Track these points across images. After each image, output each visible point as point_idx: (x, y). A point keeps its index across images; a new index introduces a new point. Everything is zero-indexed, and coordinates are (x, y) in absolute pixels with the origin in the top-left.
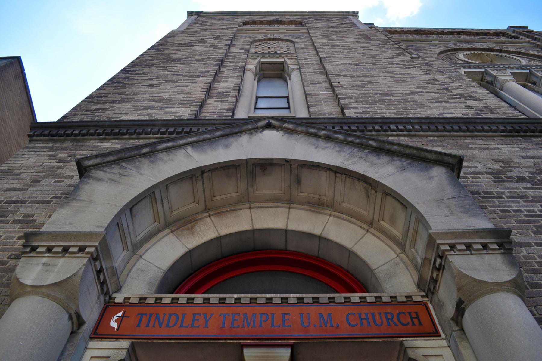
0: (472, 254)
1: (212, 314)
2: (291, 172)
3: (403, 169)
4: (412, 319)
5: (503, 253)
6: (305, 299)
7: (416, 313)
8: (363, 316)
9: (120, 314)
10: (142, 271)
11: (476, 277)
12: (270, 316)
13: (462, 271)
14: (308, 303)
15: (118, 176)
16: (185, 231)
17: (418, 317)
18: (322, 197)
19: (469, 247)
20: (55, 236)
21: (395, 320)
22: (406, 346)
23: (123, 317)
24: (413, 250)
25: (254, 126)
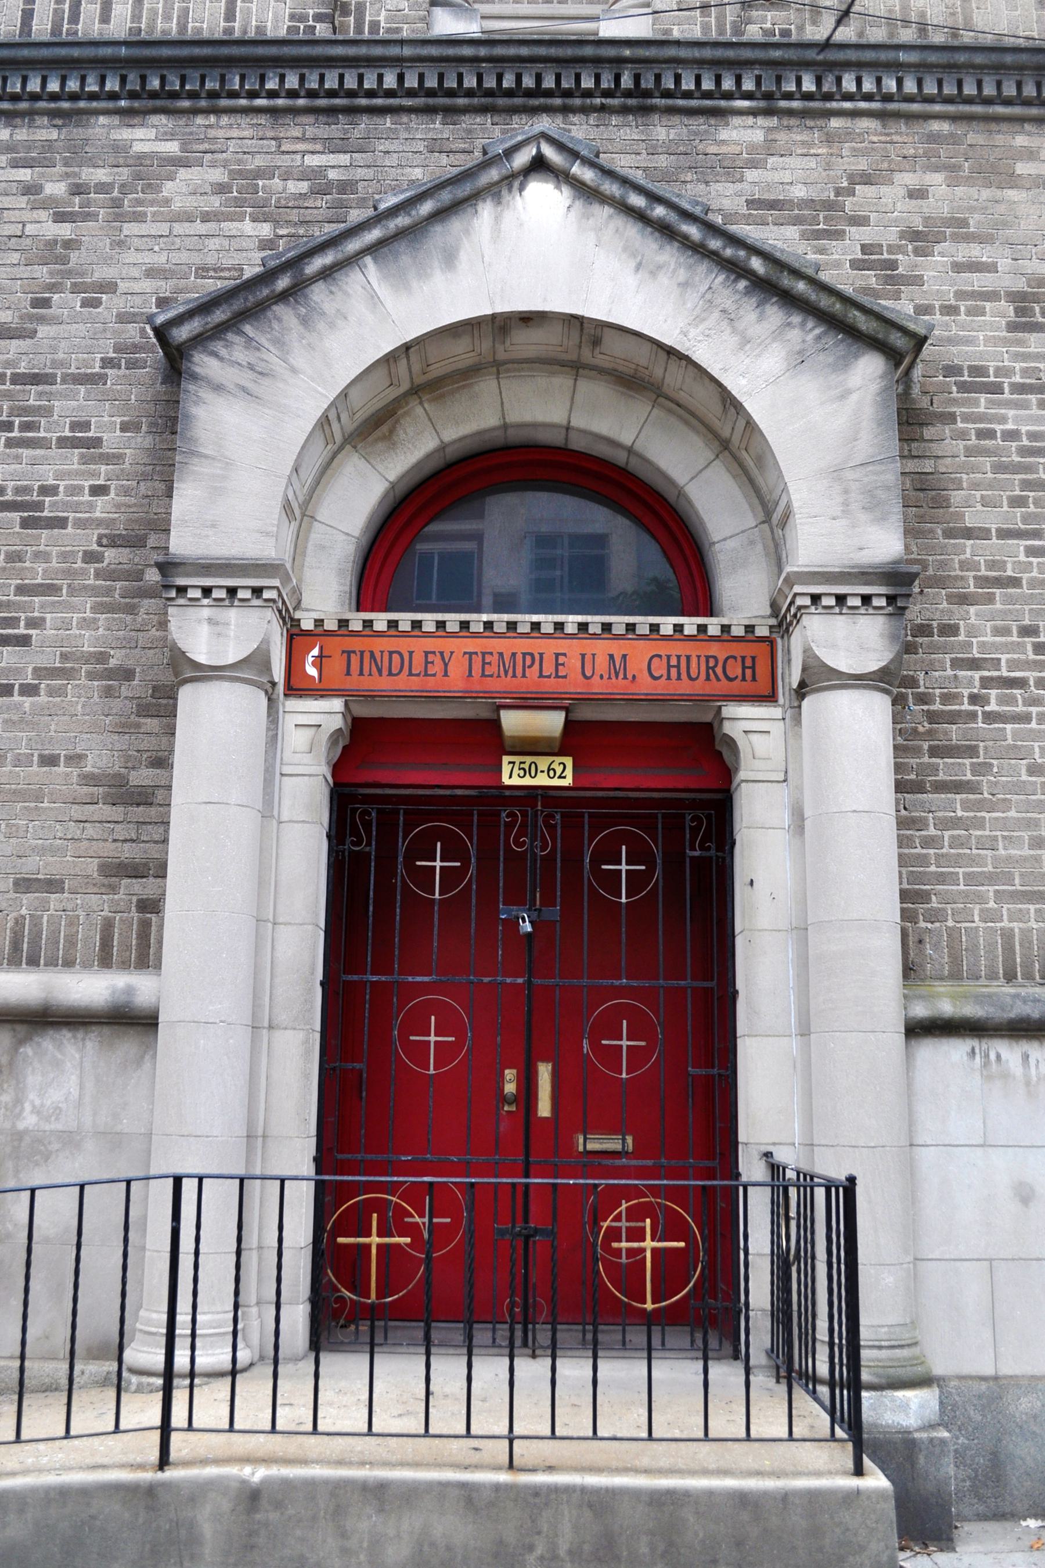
0: (841, 614)
1: (452, 653)
2: (582, 330)
3: (800, 360)
4: (744, 668)
5: (890, 614)
6: (590, 626)
7: (753, 658)
8: (674, 662)
9: (315, 652)
10: (323, 548)
11: (829, 663)
12: (537, 657)
13: (814, 648)
14: (595, 634)
15: (250, 375)
16: (380, 444)
17: (753, 668)
18: (640, 369)
19: (841, 599)
20: (208, 568)
21: (719, 670)
22: (723, 716)
23: (321, 656)
24: (780, 531)
25: (504, 172)
